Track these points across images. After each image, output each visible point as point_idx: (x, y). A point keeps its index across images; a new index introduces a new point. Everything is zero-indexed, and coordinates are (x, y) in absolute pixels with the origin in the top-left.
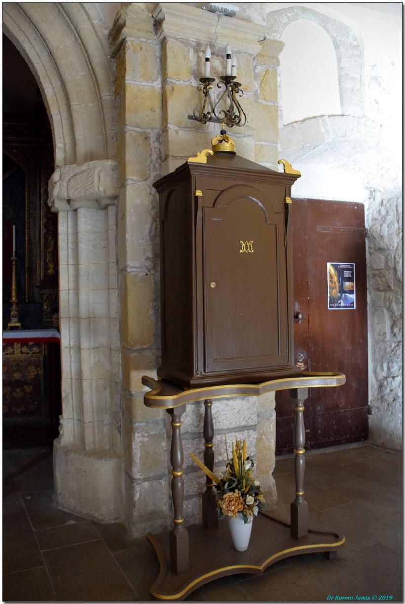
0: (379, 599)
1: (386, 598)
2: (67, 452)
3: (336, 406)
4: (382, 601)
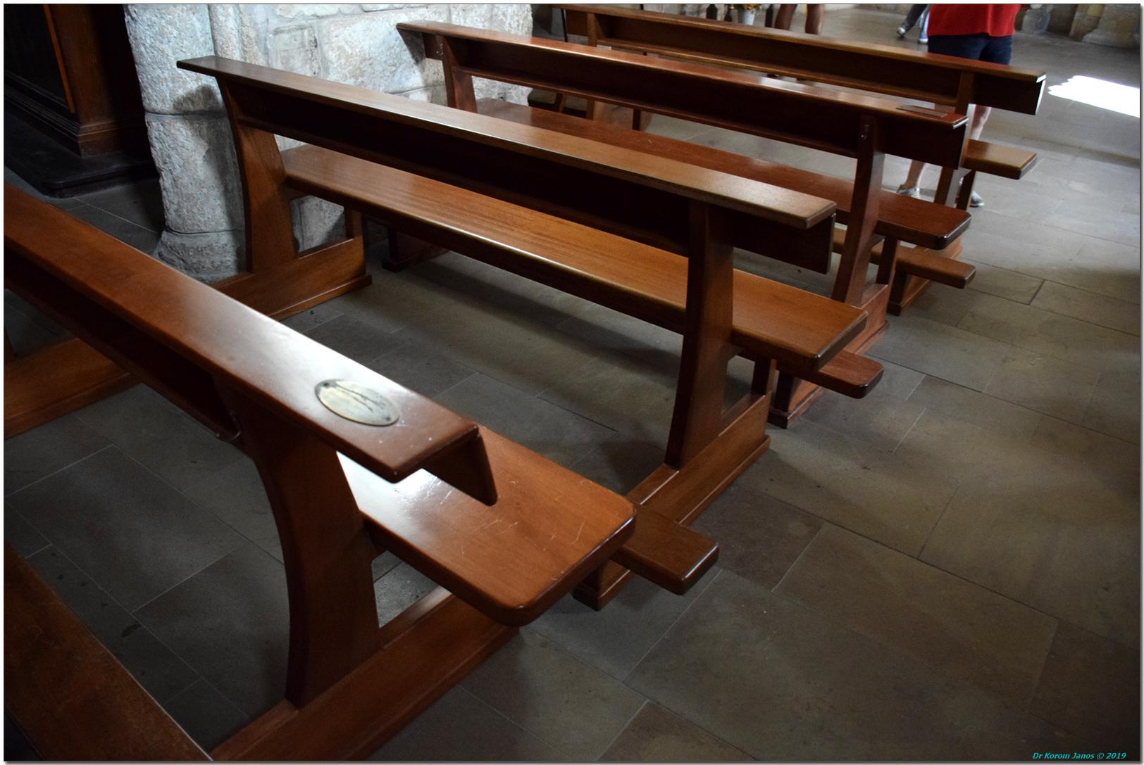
0: (1107, 758)
1: (1117, 756)
4: (1111, 760)
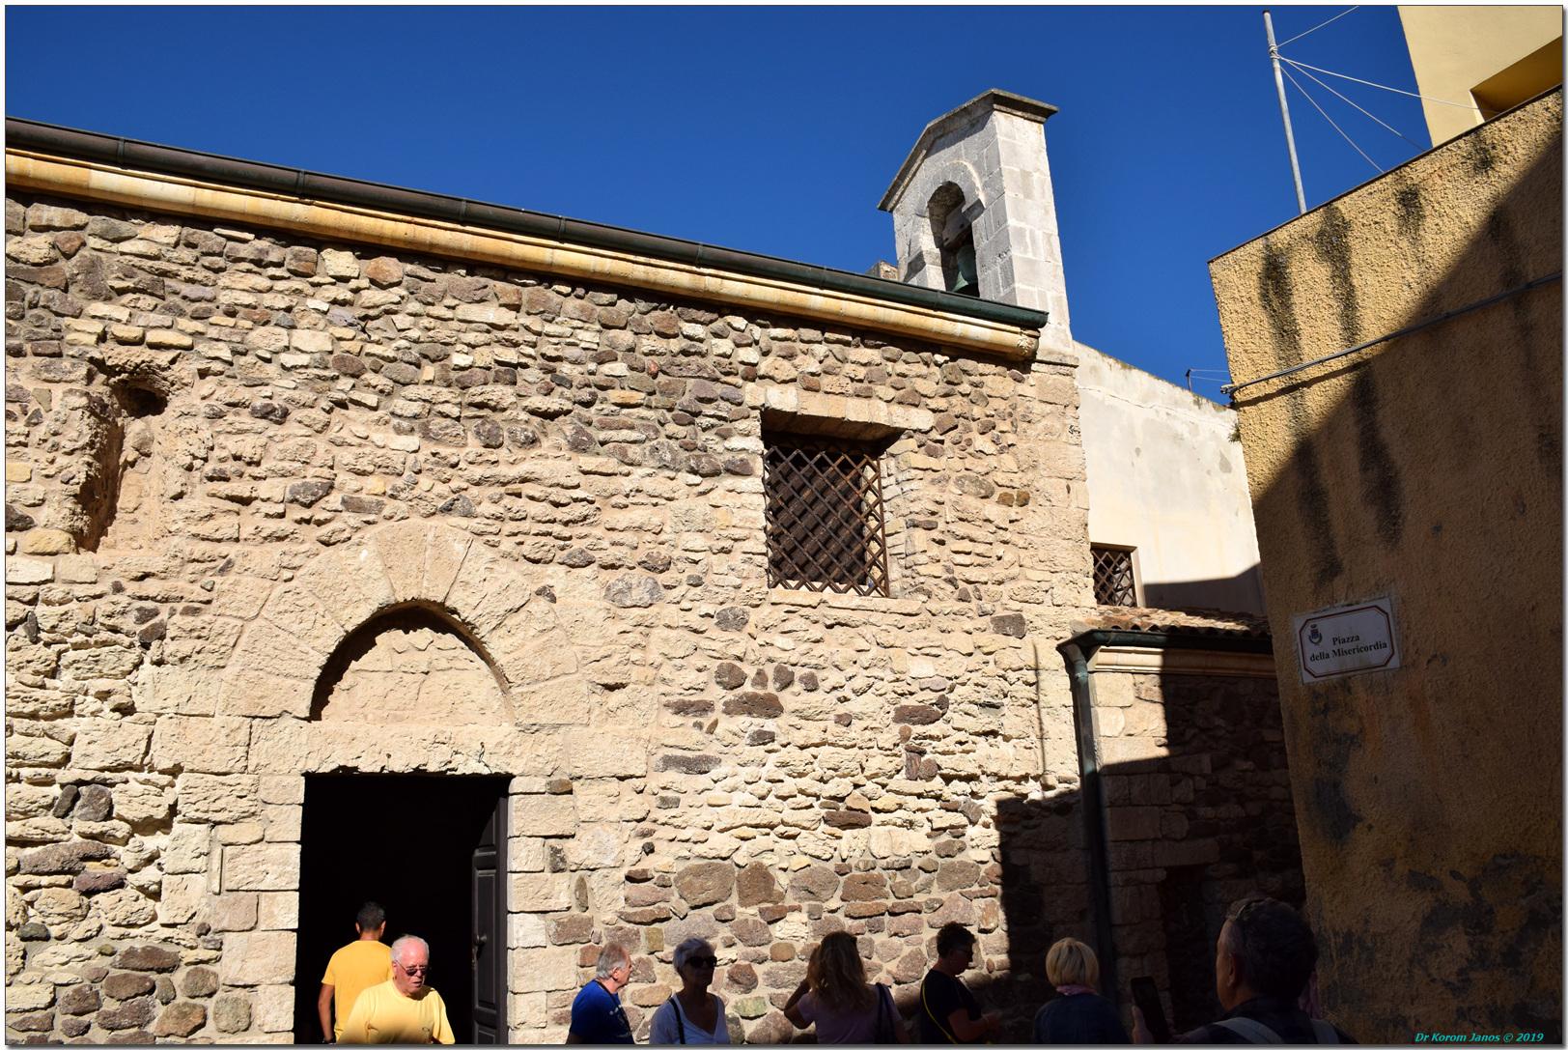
2: (772, 850)
3: (1521, 954)
4: (1523, 1043)
